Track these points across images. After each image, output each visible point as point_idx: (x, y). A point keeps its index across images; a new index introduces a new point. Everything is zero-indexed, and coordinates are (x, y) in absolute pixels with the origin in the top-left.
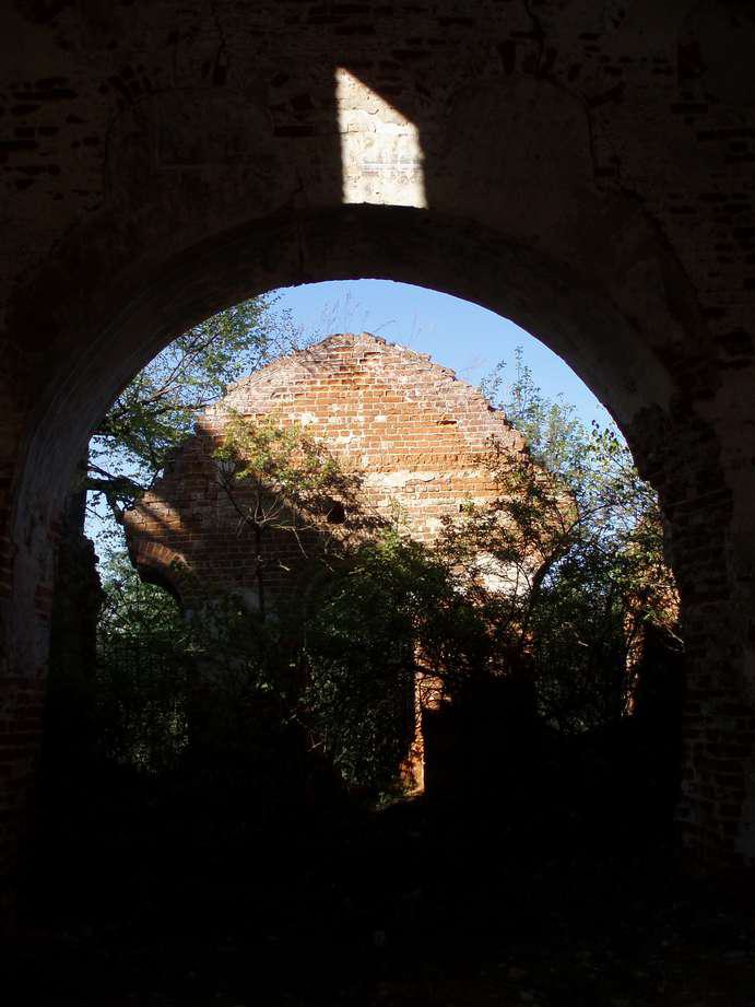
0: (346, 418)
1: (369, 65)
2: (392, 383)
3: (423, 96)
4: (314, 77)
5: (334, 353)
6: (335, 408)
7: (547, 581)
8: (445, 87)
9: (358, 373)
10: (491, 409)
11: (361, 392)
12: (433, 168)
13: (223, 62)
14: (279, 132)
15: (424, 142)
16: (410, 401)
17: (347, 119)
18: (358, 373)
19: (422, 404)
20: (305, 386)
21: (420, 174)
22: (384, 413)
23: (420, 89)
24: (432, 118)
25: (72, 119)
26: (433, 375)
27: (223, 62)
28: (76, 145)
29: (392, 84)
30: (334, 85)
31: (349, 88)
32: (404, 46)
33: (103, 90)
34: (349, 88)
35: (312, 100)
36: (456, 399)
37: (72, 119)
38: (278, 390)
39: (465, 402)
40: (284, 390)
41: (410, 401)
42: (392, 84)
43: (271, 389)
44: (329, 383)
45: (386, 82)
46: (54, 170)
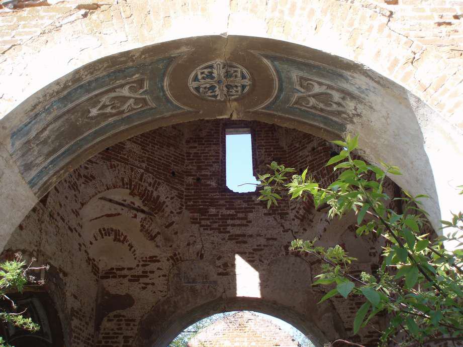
0: (241, 343)
1: (245, 253)
2: (257, 331)
3: (261, 263)
4: (229, 257)
5: (237, 319)
6: (237, 339)
7: (99, 302)
8: (267, 260)
9: (245, 327)
10: (293, 340)
11: (246, 334)
12: (263, 285)
13: (203, 252)
14: (219, 274)
15: (261, 277)
16: (264, 337)
17: (238, 270)
18: (245, 327)
19: (268, 338)
20: (226, 331)
21: (259, 287)
22: (255, 341)
23: (260, 261)
24: (264, 270)
25: (158, 269)
26: (272, 328)
27: (203, 252)
28: (159, 277)
29: (252, 259)
30: (234, 259)
31: (238, 258)
32: (256, 247)
33: (168, 260)
34: (238, 258)
35: (229, 264)
36: (280, 336)
37: (158, 269)
38: (217, 332)
39: (284, 338)
40: (219, 332)
41: (264, 337)
42: (252, 259)
43: (214, 332)
44: (235, 330)
45: (250, 259)
46: (153, 284)
